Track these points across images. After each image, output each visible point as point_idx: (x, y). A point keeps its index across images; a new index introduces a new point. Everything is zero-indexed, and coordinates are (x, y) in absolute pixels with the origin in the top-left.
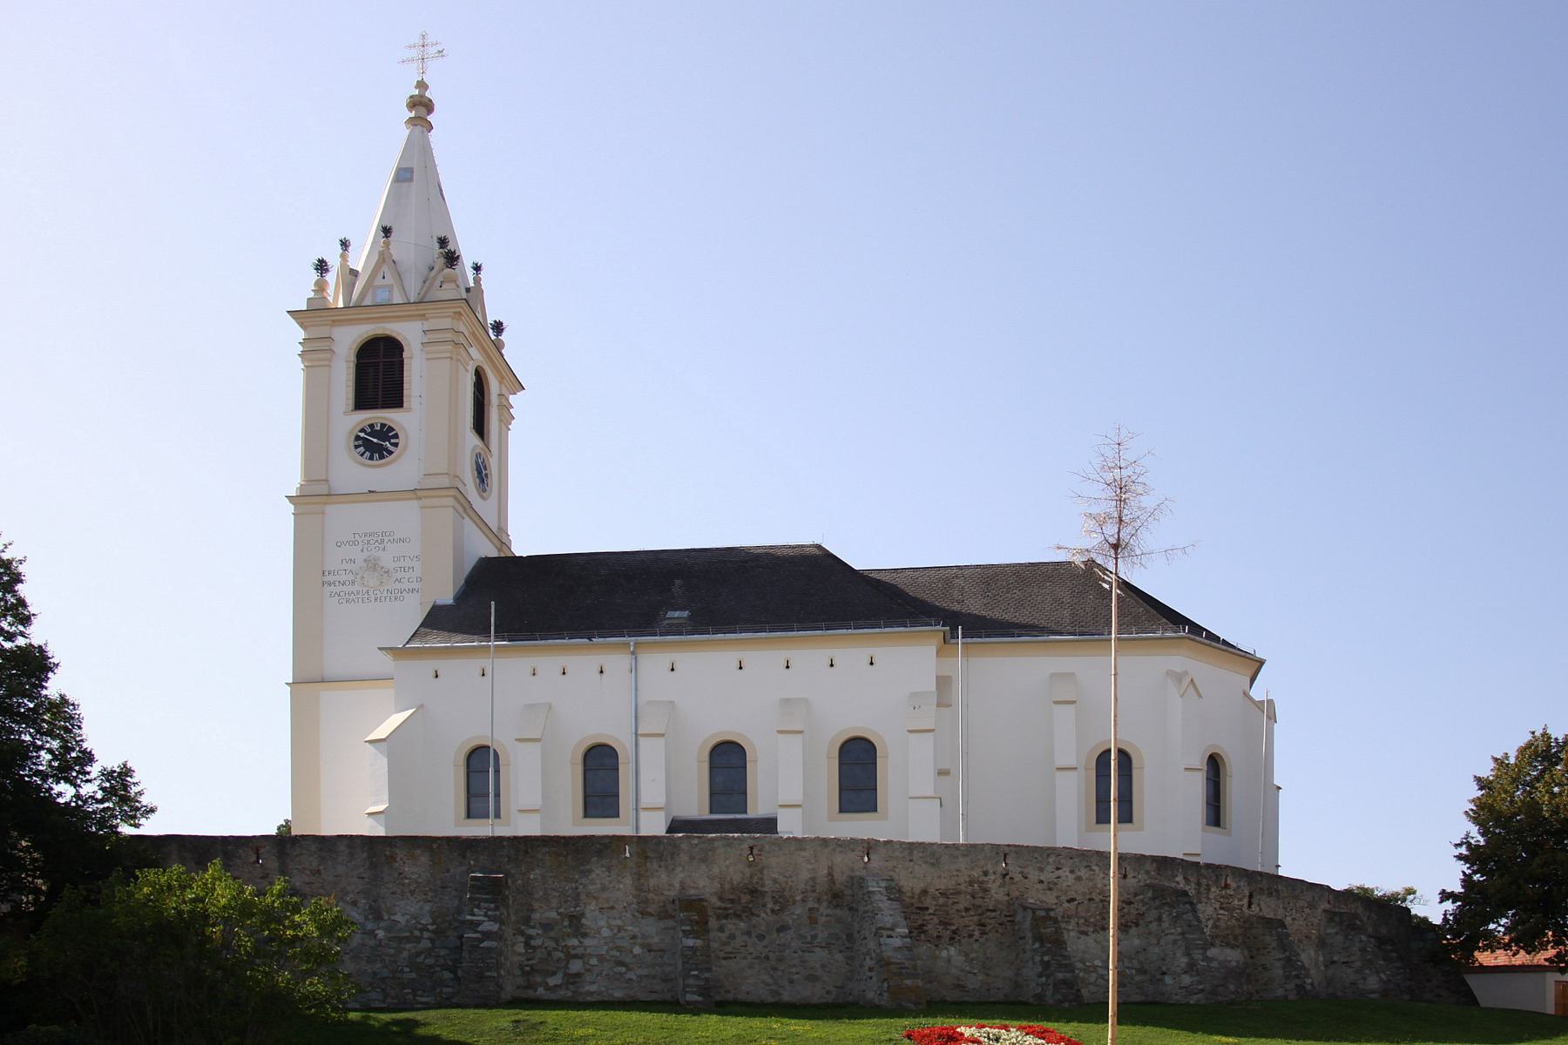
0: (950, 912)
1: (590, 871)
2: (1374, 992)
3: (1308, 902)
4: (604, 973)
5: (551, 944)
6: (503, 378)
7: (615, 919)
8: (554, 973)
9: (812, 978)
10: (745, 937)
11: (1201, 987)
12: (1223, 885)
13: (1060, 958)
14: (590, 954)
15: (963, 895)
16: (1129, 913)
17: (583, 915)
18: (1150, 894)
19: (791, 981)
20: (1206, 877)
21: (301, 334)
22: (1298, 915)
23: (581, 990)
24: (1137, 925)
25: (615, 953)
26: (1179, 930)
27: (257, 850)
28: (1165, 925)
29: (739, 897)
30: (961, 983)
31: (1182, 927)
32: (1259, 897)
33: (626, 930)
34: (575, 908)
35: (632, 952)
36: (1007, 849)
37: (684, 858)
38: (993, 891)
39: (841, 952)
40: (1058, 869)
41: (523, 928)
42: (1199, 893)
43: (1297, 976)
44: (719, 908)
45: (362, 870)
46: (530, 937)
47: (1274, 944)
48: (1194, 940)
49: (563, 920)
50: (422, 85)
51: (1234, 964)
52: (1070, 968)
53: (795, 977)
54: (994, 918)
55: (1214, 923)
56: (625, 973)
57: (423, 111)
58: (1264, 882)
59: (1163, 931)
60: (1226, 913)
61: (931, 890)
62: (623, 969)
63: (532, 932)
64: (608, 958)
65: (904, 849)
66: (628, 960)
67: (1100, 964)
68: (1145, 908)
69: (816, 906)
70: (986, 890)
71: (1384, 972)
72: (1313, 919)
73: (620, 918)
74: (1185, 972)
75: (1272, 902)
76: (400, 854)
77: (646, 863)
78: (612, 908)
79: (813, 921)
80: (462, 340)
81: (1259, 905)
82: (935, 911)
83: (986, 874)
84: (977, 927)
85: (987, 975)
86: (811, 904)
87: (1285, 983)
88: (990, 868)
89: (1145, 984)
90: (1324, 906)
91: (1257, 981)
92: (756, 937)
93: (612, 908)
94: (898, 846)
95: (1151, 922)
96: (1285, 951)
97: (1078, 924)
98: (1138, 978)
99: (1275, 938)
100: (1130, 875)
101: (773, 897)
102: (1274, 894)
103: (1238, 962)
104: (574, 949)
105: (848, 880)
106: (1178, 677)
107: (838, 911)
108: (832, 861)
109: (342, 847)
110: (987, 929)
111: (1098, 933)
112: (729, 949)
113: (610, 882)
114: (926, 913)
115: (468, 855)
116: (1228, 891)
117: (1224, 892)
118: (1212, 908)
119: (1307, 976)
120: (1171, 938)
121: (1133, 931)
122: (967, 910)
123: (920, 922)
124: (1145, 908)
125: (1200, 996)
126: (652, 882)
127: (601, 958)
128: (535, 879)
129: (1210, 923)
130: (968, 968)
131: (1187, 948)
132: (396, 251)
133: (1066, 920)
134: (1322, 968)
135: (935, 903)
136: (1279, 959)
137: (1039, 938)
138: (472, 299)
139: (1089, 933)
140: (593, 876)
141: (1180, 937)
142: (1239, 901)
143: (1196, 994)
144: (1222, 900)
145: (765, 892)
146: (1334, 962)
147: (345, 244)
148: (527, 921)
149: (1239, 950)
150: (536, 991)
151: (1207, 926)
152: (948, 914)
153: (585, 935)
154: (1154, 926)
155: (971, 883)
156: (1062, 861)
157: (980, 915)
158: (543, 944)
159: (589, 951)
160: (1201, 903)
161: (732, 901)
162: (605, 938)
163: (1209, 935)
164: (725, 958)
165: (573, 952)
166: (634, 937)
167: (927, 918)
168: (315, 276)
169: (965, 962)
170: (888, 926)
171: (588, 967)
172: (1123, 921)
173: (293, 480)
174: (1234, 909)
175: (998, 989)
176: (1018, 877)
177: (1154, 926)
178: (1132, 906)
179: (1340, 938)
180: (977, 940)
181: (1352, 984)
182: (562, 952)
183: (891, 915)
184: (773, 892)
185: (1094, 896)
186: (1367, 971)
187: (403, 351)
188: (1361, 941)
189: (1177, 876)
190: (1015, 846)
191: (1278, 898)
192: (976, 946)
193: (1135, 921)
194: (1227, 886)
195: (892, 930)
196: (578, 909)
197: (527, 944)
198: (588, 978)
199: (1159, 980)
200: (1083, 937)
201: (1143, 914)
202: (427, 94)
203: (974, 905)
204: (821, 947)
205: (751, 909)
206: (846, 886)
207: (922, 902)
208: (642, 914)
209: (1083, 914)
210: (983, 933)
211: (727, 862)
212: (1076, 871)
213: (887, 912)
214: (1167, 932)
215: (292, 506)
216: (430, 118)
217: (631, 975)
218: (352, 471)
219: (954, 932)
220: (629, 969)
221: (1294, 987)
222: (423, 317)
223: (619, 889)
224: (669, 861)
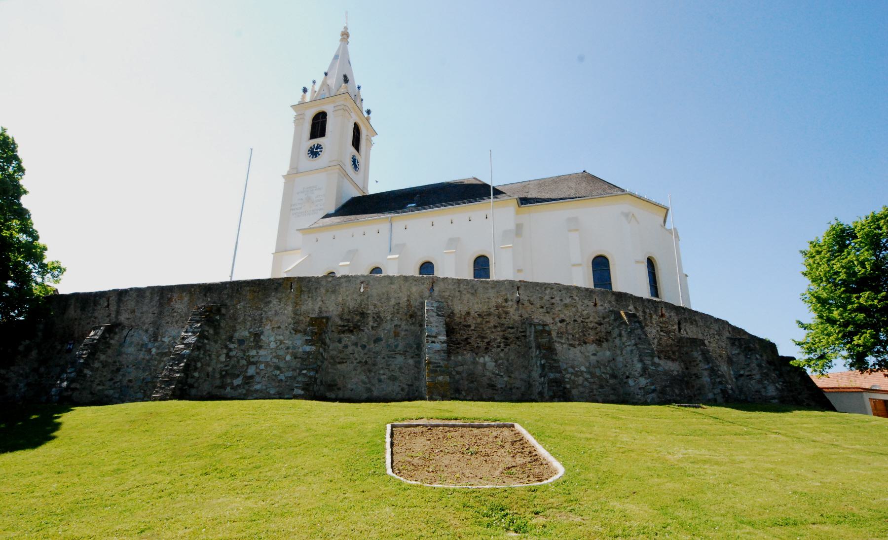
0: (485, 329)
1: (270, 302)
2: (774, 398)
3: (717, 331)
4: (267, 375)
5: (240, 354)
7: (280, 335)
8: (238, 376)
9: (393, 379)
10: (354, 347)
11: (653, 387)
13: (552, 362)
14: (260, 361)
15: (492, 316)
16: (601, 331)
17: (262, 333)
18: (612, 318)
19: (380, 381)
20: (649, 309)
23: (251, 389)
24: (607, 340)
25: (275, 360)
26: (633, 342)
27: (109, 299)
28: (624, 339)
29: (353, 317)
31: (635, 339)
32: (684, 324)
33: (284, 343)
34: (258, 328)
35: (285, 359)
36: (519, 284)
37: (323, 291)
38: (511, 314)
39: (412, 357)
41: (228, 343)
42: (645, 319)
43: (720, 383)
44: (340, 326)
45: (155, 308)
46: (230, 350)
47: (700, 358)
48: (644, 348)
49: (250, 337)
50: (346, 28)
51: (675, 373)
52: (558, 370)
53: (382, 377)
55: (658, 342)
56: (279, 375)
58: (686, 313)
59: (623, 344)
60: (665, 334)
61: (472, 313)
62: (278, 372)
63: (232, 346)
64: (271, 364)
65: (455, 283)
66: (282, 365)
67: (585, 370)
68: (611, 328)
69: (399, 323)
70: (507, 313)
71: (778, 382)
72: (722, 344)
73: (283, 335)
74: (641, 376)
75: (694, 329)
76: (175, 296)
77: (301, 295)
78: (279, 327)
79: (397, 335)
80: (347, 108)
81: (685, 330)
82: (475, 328)
83: (506, 301)
84: (503, 340)
85: (510, 377)
86: (396, 322)
87: (713, 389)
88: (509, 297)
89: (617, 386)
90: (727, 334)
91: (693, 387)
92: (361, 346)
93: (279, 327)
94: (450, 281)
95: (615, 338)
96: (708, 363)
97: (568, 338)
98: (611, 381)
99: (699, 353)
100: (599, 303)
101: (374, 317)
102: (694, 323)
103: (678, 371)
104: (252, 358)
105: (419, 304)
106: (626, 215)
107: (413, 327)
108: (410, 292)
109: (148, 294)
110: (509, 342)
111: (582, 345)
112: (341, 356)
113: (280, 309)
115: (208, 295)
118: (655, 331)
119: (727, 382)
120: (629, 348)
121: (605, 345)
122: (495, 327)
123: (465, 337)
124: (611, 328)
125: (653, 395)
126: (304, 308)
127: (267, 364)
128: (240, 308)
129: (656, 341)
130: (497, 372)
131: (640, 356)
132: (329, 82)
133: (559, 335)
134: (734, 380)
135: (474, 322)
136: (706, 369)
137: (539, 347)
138: (356, 99)
139: (576, 346)
140: (271, 305)
141: (634, 347)
143: (651, 393)
144: (661, 325)
145: (369, 314)
146: (741, 375)
147: (314, 82)
148: (231, 339)
149: (678, 363)
150: (225, 390)
151: (654, 343)
152: (483, 330)
153: (260, 347)
154: (617, 341)
155: (497, 307)
156: (555, 293)
157: (504, 331)
158: (236, 354)
159: (260, 359)
160: (648, 326)
161: (348, 321)
162: (272, 349)
163: (656, 351)
164: (339, 363)
165: (252, 360)
166: (288, 348)
167: (470, 333)
168: (302, 93)
169: (495, 366)
170: (434, 334)
171: (258, 370)
172: (597, 337)
173: (285, 169)
174: (670, 332)
175: (517, 388)
176: (527, 304)
177: (617, 341)
179: (742, 357)
180: (502, 350)
181: (756, 391)
182: (246, 360)
183: (436, 326)
184: (373, 313)
186: (766, 382)
188: (757, 359)
189: (629, 306)
190: (524, 282)
191: (697, 326)
192: (502, 355)
193: (605, 337)
194: (662, 315)
195: (435, 337)
196: (260, 329)
197: (227, 355)
198: (258, 379)
199: (626, 383)
201: (610, 333)
203: (499, 323)
204: (400, 354)
205: (359, 326)
206: (418, 309)
207: (467, 322)
208: (296, 331)
209: (571, 332)
210: (507, 345)
211: (347, 293)
212: (564, 300)
213: (434, 324)
214: (626, 344)
217: (282, 377)
218: (307, 163)
219: (488, 343)
220: (282, 373)
221: (720, 391)
223: (284, 314)
224: (314, 294)
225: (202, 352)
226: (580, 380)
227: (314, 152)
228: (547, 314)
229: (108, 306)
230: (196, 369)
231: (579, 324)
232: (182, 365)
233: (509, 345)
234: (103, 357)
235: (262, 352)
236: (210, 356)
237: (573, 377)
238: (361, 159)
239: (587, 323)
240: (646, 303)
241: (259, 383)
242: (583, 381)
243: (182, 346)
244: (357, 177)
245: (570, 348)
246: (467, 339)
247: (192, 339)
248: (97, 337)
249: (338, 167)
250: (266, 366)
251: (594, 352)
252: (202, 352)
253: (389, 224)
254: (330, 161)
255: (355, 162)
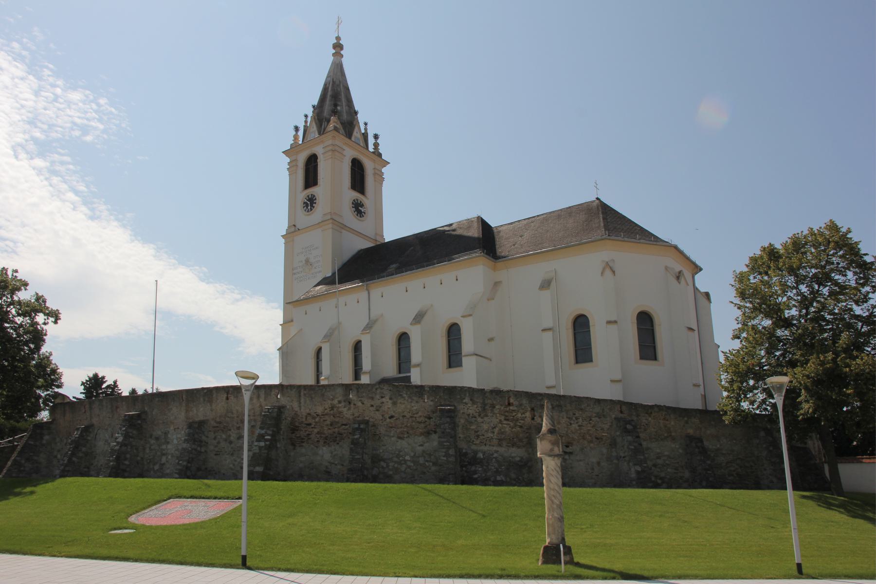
1: (171, 409)
6: (374, 160)
12: (507, 404)
21: (288, 160)
22: (585, 423)
30: (328, 470)
38: (345, 413)
40: (382, 397)
50: (338, 38)
51: (518, 459)
54: (346, 429)
57: (338, 49)
67: (409, 459)
78: (178, 428)
82: (315, 426)
93: (178, 428)
114: (311, 427)
116: (511, 408)
117: (508, 408)
142: (522, 414)
144: (506, 414)
153: (168, 443)
165: (164, 452)
178: (432, 420)
185: (405, 414)
187: (317, 158)
193: (434, 430)
200: (400, 441)
202: (341, 42)
215: (284, 240)
216: (342, 52)
218: (305, 219)
222: (322, 142)
225: (129, 447)
226: (403, 468)
227: (310, 203)
228: (377, 412)
229: (85, 412)
230: (126, 459)
231: (408, 419)
232: (114, 457)
233: (344, 439)
234: (84, 449)
235: (169, 446)
236: (137, 449)
237: (396, 465)
238: (367, 202)
239: (416, 417)
240: (487, 394)
241: (169, 468)
242: (406, 469)
243: (115, 444)
244: (364, 226)
245: (399, 440)
246: (309, 435)
247: (120, 439)
248: (77, 436)
249: (331, 221)
250: (172, 456)
251: (421, 443)
252: (129, 447)
253: (367, 292)
254: (325, 215)
255: (358, 208)
